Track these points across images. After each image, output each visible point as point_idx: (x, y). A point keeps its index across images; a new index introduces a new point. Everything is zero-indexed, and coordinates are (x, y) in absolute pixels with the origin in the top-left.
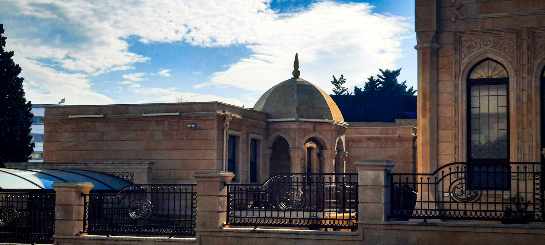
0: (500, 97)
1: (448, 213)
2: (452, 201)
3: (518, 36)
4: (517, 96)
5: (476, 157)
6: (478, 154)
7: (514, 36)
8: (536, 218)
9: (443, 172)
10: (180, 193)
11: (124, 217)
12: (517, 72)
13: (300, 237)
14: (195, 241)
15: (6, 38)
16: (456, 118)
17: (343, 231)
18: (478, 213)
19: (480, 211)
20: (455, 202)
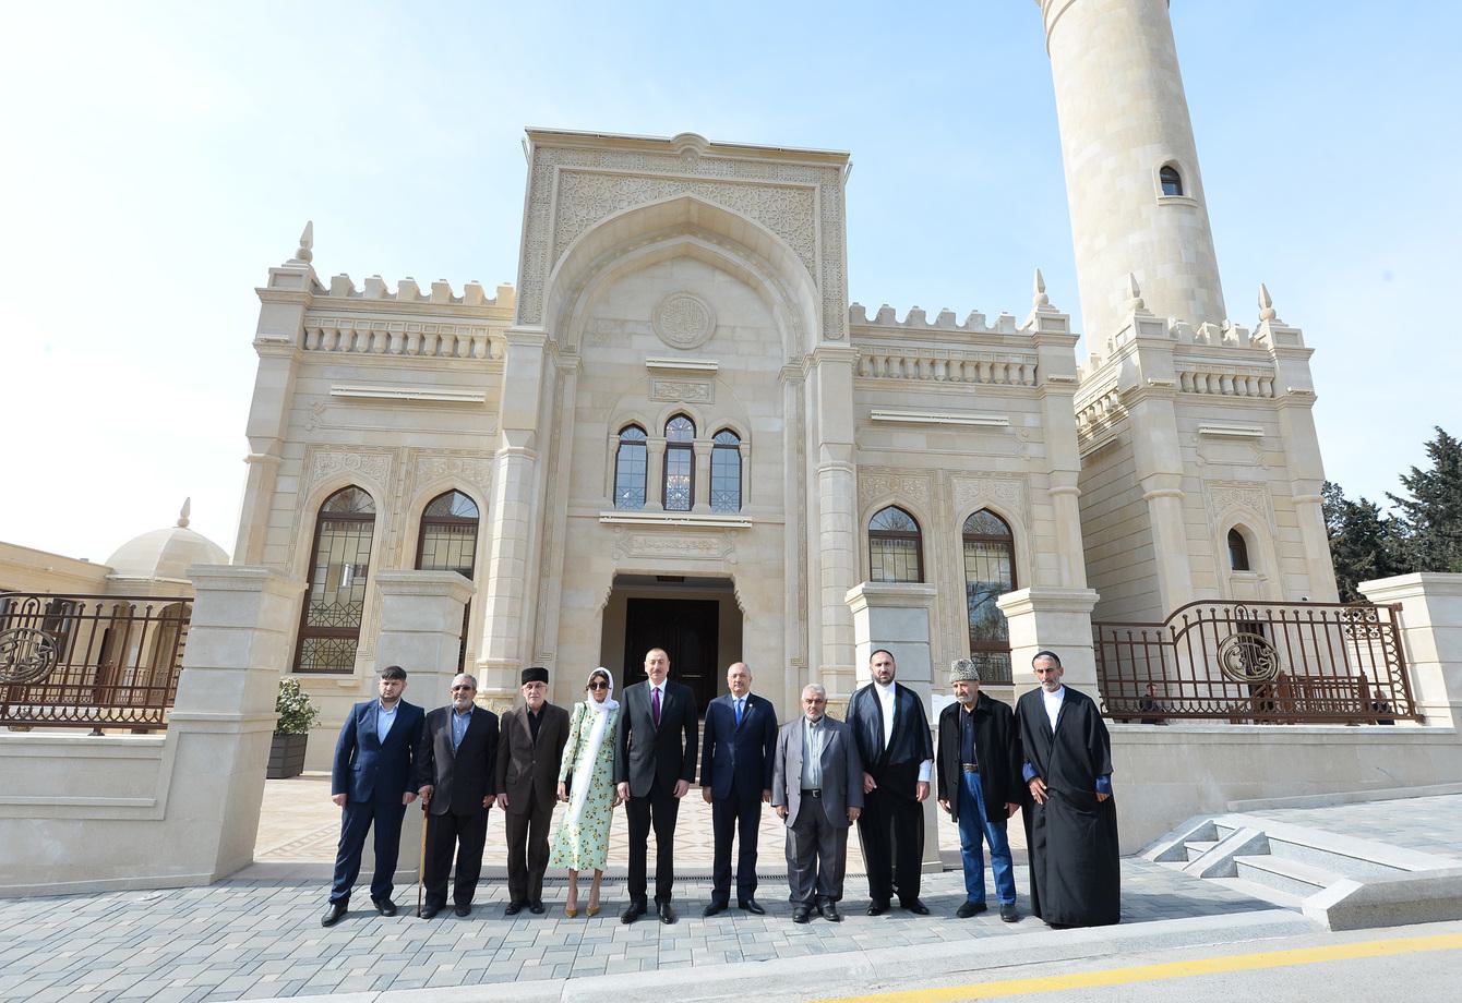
0: (439, 541)
1: (1177, 704)
2: (1226, 679)
3: (396, 457)
4: (383, 538)
5: (313, 624)
6: (345, 620)
7: (390, 457)
8: (1400, 711)
9: (1173, 628)
10: (1131, 643)
11: (1343, 683)
12: (387, 505)
13: (1325, 740)
14: (161, 746)
15: (258, 291)
16: (289, 565)
17: (111, 735)
18: (1223, 704)
19: (1196, 698)
20: (1232, 682)
